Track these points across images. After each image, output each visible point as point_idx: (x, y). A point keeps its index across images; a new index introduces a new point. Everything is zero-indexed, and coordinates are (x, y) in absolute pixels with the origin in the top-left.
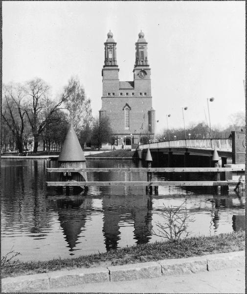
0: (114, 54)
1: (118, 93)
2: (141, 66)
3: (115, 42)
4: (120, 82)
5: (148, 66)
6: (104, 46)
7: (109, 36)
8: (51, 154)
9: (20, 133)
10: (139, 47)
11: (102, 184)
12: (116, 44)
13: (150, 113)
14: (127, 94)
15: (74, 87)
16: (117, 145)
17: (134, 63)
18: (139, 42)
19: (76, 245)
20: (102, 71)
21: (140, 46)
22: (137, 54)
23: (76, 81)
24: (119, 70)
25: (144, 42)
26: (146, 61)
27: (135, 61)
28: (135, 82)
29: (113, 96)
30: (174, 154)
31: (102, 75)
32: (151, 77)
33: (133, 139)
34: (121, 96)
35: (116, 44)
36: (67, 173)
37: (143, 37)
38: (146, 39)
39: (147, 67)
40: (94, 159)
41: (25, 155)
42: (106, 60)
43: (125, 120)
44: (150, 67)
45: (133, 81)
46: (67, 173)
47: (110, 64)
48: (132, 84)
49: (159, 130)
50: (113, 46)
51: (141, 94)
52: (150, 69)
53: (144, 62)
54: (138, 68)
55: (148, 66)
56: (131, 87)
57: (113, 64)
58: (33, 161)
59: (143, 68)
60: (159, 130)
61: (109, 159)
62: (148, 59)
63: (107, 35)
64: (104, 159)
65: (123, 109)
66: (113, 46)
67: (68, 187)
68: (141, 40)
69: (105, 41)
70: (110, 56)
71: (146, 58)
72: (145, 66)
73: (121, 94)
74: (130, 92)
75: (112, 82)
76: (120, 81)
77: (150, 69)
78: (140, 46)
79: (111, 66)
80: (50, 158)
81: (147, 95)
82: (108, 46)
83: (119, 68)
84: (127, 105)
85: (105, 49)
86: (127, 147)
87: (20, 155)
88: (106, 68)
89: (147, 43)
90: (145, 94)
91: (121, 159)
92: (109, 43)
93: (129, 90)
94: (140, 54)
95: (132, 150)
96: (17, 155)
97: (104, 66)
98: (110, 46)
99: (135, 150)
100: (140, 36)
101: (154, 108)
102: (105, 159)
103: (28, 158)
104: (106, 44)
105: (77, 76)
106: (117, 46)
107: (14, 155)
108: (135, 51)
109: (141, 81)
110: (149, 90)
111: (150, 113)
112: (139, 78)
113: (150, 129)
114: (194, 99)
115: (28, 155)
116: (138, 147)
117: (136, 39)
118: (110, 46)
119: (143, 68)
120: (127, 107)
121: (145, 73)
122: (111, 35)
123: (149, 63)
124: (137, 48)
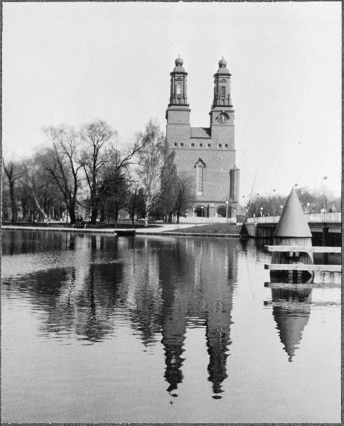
0: (184, 88)
1: (188, 143)
2: (221, 107)
3: (186, 71)
4: (191, 128)
5: (232, 106)
6: (170, 77)
7: (178, 63)
8: (119, 226)
9: (72, 196)
10: (220, 79)
11: (289, 267)
12: (186, 74)
13: (232, 173)
14: (201, 145)
15: (153, 135)
16: (208, 216)
17: (211, 103)
18: (220, 72)
19: (183, 363)
20: (167, 112)
21: (221, 77)
22: (216, 89)
23: (156, 125)
24: (190, 111)
25: (226, 73)
26: (228, 99)
27: (213, 99)
28: (213, 128)
29: (226, 149)
30: (330, 231)
31: (167, 118)
32: (236, 122)
33: (208, 208)
34: (201, 148)
35: (186, 74)
36: (294, 253)
37: (181, 64)
38: (229, 68)
39: (230, 109)
40: (185, 235)
41: (82, 227)
42: (173, 96)
43: (198, 182)
44: (189, 108)
45: (209, 127)
46: (294, 253)
47: (178, 102)
48: (209, 131)
49: (244, 199)
50: (182, 78)
51: (220, 145)
52: (233, 112)
53: (226, 101)
54: (217, 108)
55: (232, 106)
56: (207, 136)
57: (182, 102)
58: (47, 232)
59: (224, 109)
60: (244, 197)
61: (204, 236)
62: (231, 97)
63: (218, 62)
64: (199, 235)
65: (195, 167)
66: (182, 78)
67: (295, 272)
68: (223, 71)
69: (172, 71)
70: (179, 91)
71: (229, 96)
72: (178, 105)
73: (193, 145)
74: (205, 143)
75: (178, 127)
76: (191, 126)
77: (233, 112)
78: (221, 77)
79: (180, 105)
80: (115, 232)
81: (228, 146)
82: (176, 78)
83: (189, 108)
84: (200, 160)
85: (172, 81)
86: (223, 220)
87: (74, 227)
88: (172, 107)
89: (230, 75)
90: (226, 145)
91: (223, 236)
92: (178, 73)
93: (204, 140)
94: (221, 91)
95: (238, 224)
96: (71, 227)
97: (170, 105)
98: (178, 76)
99: (241, 224)
100: (221, 65)
101: (238, 166)
102: (200, 235)
103: (86, 232)
104: (173, 74)
105: (156, 119)
106: (188, 78)
107: (65, 227)
108: (213, 85)
109: (220, 128)
110: (232, 140)
111: (232, 173)
112: (218, 124)
113: (232, 195)
114: (285, 158)
115: (87, 227)
116: (246, 221)
117: (216, 69)
118: (178, 76)
119: (224, 109)
120: (200, 163)
121: (227, 117)
122: (180, 61)
123: (232, 102)
124: (217, 82)
